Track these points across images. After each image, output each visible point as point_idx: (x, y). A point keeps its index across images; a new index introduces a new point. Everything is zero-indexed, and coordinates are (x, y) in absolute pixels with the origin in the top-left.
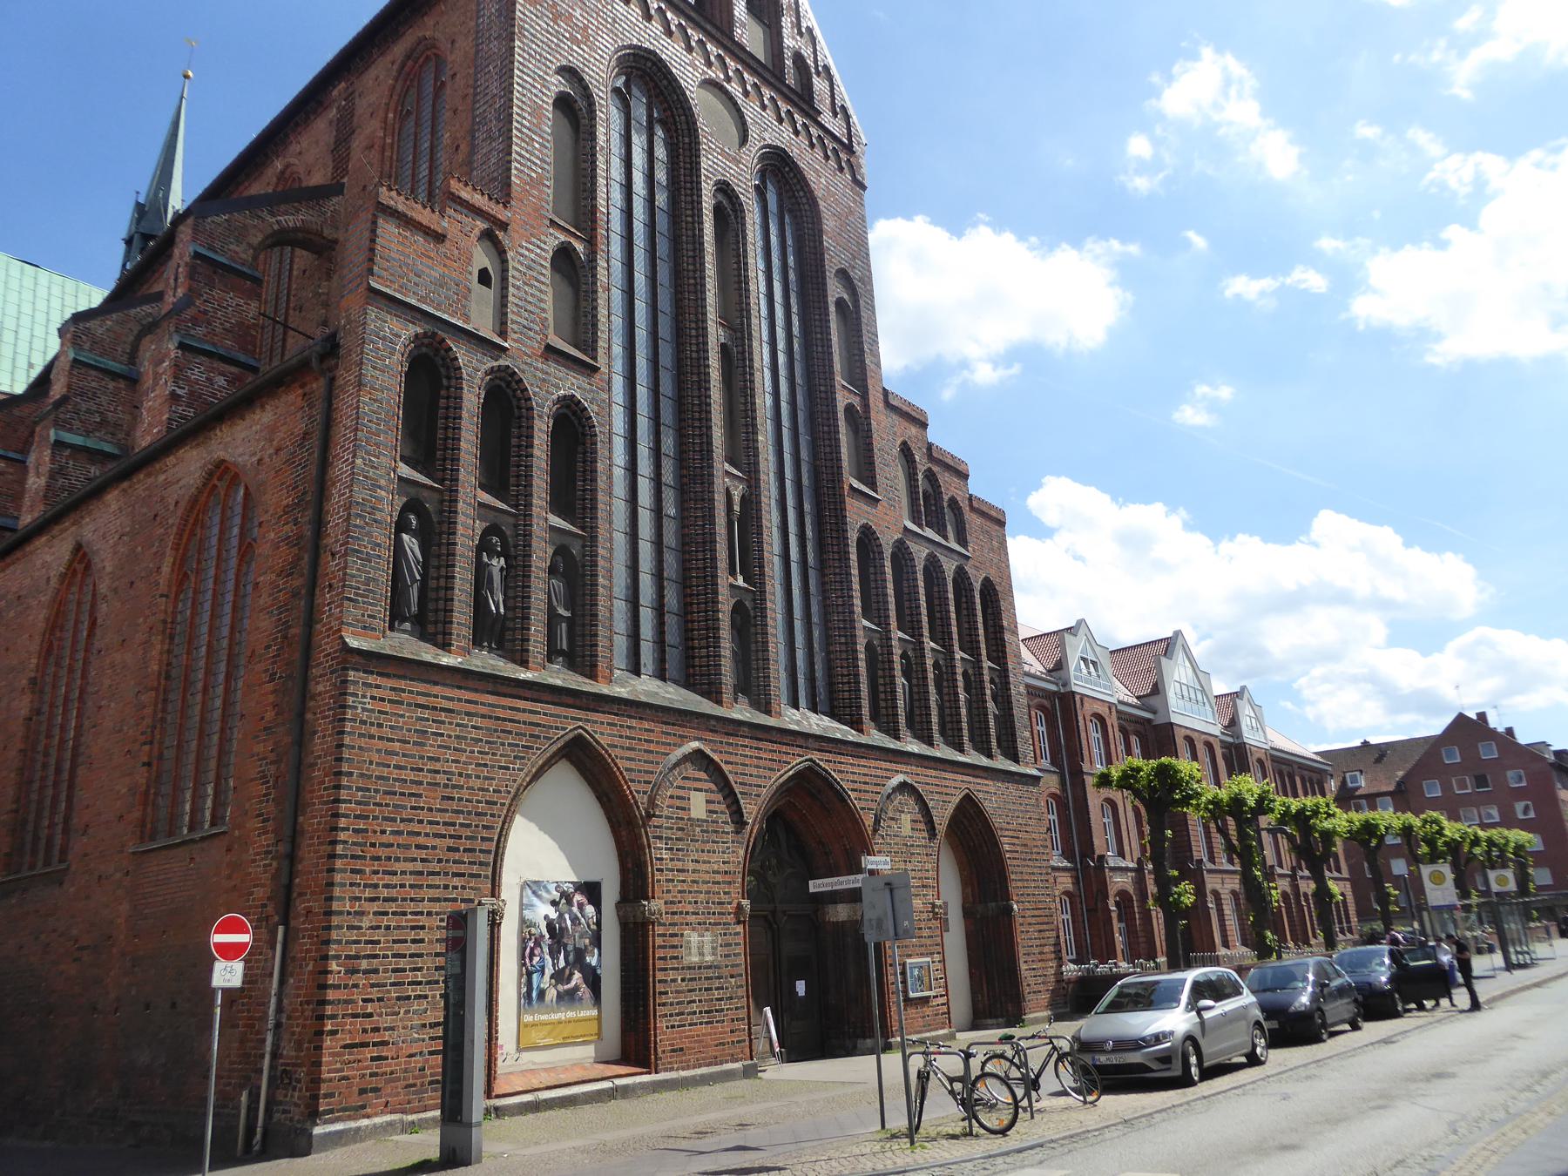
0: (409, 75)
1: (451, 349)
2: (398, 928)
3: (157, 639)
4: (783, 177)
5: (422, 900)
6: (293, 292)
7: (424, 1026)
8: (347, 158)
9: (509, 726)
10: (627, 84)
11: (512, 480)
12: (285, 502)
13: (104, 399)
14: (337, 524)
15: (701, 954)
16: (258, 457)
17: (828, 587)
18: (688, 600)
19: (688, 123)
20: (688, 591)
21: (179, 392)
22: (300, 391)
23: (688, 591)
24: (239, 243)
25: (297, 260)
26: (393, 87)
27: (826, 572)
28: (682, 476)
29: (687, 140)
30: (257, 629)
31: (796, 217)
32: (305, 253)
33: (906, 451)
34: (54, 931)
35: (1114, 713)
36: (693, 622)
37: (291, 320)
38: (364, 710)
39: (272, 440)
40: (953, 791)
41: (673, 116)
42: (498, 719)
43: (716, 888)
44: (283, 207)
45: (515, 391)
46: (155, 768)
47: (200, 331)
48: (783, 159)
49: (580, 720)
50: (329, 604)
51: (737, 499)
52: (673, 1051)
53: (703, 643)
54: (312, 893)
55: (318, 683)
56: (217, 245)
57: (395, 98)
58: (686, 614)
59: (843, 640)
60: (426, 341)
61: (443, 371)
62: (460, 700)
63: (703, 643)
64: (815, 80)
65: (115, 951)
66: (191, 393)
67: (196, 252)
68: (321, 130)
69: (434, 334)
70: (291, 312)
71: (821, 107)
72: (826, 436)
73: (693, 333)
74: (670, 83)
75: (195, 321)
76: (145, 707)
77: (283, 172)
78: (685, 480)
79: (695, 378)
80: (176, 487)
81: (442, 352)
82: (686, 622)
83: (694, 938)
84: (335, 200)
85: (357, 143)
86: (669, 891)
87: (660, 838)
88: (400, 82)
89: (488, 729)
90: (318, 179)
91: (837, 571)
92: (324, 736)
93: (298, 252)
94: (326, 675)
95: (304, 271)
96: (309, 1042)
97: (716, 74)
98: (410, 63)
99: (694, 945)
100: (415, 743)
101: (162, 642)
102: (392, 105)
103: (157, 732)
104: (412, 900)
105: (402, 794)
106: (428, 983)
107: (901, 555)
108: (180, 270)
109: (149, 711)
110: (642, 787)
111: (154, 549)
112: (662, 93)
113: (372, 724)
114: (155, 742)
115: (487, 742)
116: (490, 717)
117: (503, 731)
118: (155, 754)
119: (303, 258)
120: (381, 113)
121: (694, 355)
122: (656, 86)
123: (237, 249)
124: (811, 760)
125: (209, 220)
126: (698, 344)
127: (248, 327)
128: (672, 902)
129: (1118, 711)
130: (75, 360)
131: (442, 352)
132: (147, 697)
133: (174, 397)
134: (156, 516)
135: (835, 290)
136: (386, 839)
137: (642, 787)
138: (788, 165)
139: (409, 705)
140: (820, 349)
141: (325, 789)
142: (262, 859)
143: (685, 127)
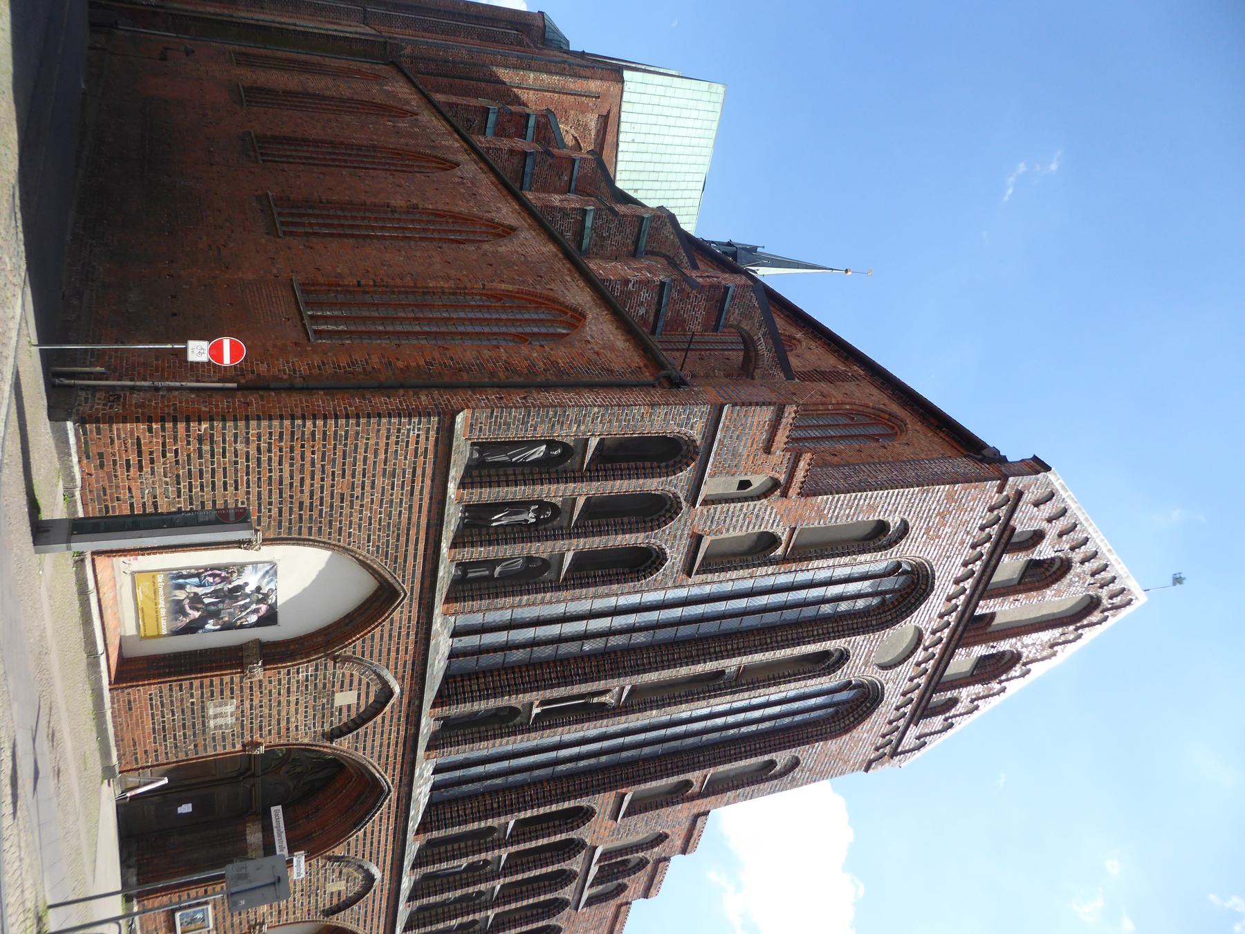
0: (878, 417)
3: (452, 284)
4: (862, 702)
5: (259, 487)
6: (712, 353)
7: (155, 497)
8: (812, 380)
9: (403, 539)
11: (596, 522)
15: (215, 717)
18: (517, 670)
21: (630, 285)
22: (642, 365)
24: (741, 314)
25: (735, 353)
29: (874, 623)
30: (465, 351)
31: (833, 717)
32: (741, 358)
36: (499, 675)
37: (693, 353)
38: (409, 430)
41: (889, 610)
42: (408, 530)
43: (274, 722)
45: (573, 849)
46: (356, 289)
47: (675, 295)
48: (876, 700)
50: (487, 398)
52: (129, 702)
53: (483, 686)
55: (427, 396)
56: (737, 301)
57: (861, 409)
58: (505, 669)
61: (671, 462)
62: (421, 500)
64: (941, 718)
66: (630, 292)
67: (729, 288)
68: (829, 362)
70: (698, 353)
75: (681, 291)
77: (795, 338)
80: (563, 289)
81: (685, 461)
83: (230, 709)
86: (270, 682)
87: (316, 670)
88: (872, 411)
89: (400, 523)
90: (794, 362)
93: (741, 354)
94: (434, 400)
98: (887, 416)
100: (385, 470)
101: (449, 288)
102: (855, 407)
103: (384, 289)
104: (259, 479)
105: (344, 464)
107: (572, 848)
108: (715, 279)
109: (398, 281)
110: (358, 649)
112: (905, 599)
113: (398, 437)
114: (376, 288)
115: (389, 523)
116: (409, 524)
117: (398, 535)
119: (737, 357)
120: (848, 400)
121: (712, 650)
123: (736, 314)
124: (390, 791)
125: (752, 294)
126: (721, 652)
127: (683, 326)
131: (685, 461)
133: (627, 282)
134: (541, 277)
135: (782, 758)
136: (308, 455)
137: (358, 649)
138: (872, 705)
139: (415, 463)
140: (733, 752)
142: (289, 368)
143: (884, 620)
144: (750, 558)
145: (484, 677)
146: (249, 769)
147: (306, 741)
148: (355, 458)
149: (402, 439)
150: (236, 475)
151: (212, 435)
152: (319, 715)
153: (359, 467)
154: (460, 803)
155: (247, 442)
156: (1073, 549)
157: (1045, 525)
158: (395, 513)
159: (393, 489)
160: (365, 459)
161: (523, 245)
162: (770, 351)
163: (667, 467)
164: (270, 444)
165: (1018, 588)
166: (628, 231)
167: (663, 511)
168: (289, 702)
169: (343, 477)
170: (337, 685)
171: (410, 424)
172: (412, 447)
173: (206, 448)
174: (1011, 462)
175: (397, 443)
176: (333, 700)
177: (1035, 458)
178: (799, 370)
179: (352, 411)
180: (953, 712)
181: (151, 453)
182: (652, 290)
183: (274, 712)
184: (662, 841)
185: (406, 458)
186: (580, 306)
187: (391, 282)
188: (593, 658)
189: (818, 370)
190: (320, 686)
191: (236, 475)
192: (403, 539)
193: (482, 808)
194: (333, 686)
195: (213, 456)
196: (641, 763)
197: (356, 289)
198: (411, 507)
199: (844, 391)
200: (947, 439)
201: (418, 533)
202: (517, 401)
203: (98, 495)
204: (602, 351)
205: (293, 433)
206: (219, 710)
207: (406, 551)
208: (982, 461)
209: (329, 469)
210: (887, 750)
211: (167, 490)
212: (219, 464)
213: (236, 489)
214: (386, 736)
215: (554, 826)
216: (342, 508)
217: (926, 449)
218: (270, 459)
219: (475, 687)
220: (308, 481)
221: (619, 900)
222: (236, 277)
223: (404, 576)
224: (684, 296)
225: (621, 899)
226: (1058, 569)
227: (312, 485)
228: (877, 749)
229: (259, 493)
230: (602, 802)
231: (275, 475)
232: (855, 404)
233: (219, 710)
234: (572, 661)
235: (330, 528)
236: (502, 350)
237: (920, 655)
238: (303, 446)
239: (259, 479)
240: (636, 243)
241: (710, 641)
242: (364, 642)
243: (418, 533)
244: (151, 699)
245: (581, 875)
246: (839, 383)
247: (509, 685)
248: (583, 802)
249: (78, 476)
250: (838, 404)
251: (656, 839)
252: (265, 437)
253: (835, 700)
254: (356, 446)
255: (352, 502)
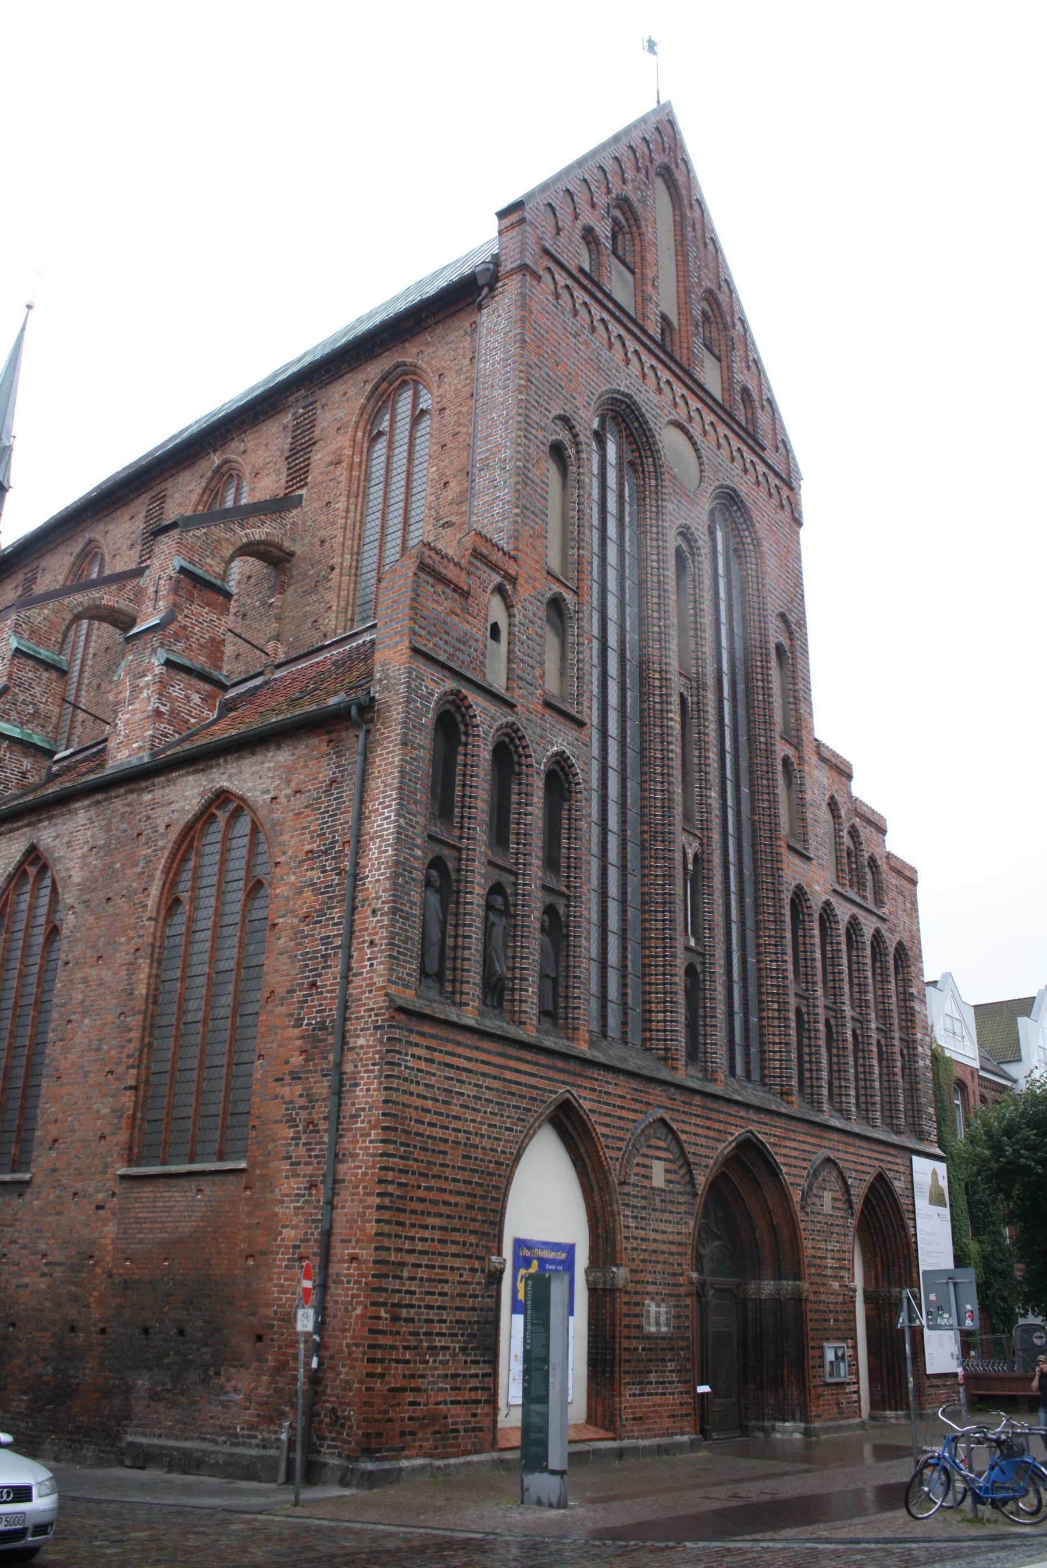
1: (465, 698)
2: (429, 1280)
3: (144, 963)
5: (447, 1255)
7: (446, 1376)
8: (305, 470)
9: (514, 1088)
10: (602, 423)
11: (512, 838)
12: (307, 848)
13: (38, 690)
14: (378, 881)
15: (658, 1324)
16: (272, 794)
17: (762, 949)
18: (647, 961)
19: (655, 465)
20: (647, 952)
21: (163, 709)
23: (647, 952)
24: (213, 556)
26: (364, 407)
27: (761, 933)
28: (643, 832)
29: (653, 482)
30: (277, 971)
33: (833, 805)
34: (14, 1242)
35: (976, 1080)
36: (650, 984)
38: (407, 1067)
39: (288, 782)
40: (867, 1169)
41: (641, 457)
42: (505, 1080)
43: (671, 1259)
44: (251, 520)
45: (517, 747)
46: (141, 1093)
47: (180, 646)
48: (732, 497)
49: (567, 1083)
50: (369, 959)
51: (690, 857)
52: (634, 1419)
53: (661, 1007)
54: (358, 1241)
55: (358, 1036)
57: (366, 417)
58: (644, 975)
59: (775, 1006)
60: (451, 698)
61: (462, 727)
62: (477, 1061)
63: (661, 1007)
64: (759, 413)
65: (98, 1270)
66: (172, 711)
69: (459, 691)
71: (765, 443)
72: (765, 790)
73: (657, 683)
74: (641, 425)
75: (177, 637)
76: (131, 1030)
77: (220, 467)
78: (646, 836)
79: (658, 731)
80: (168, 809)
82: (643, 790)
83: (653, 1308)
84: (294, 512)
85: (319, 457)
86: (633, 1260)
87: (627, 1205)
88: (372, 402)
89: (498, 1090)
91: (772, 933)
92: (368, 1090)
94: (368, 1029)
95: (249, 577)
96: (360, 1382)
97: (681, 415)
98: (384, 385)
99: (652, 1315)
100: (444, 1102)
101: (151, 966)
102: (362, 424)
103: (145, 1056)
104: (440, 1254)
105: (433, 1151)
106: (450, 1335)
107: (827, 913)
109: (135, 1035)
110: (614, 1154)
111: (139, 869)
112: (632, 434)
113: (412, 1082)
114: (143, 1066)
115: (497, 1103)
116: (499, 1079)
117: (510, 1093)
118: (143, 1077)
121: (658, 706)
122: (628, 428)
123: (212, 563)
124: (750, 1132)
126: (661, 695)
128: (636, 1271)
129: (980, 1077)
130: (17, 650)
132: (135, 1021)
133: (158, 713)
134: (139, 834)
136: (421, 1193)
137: (614, 1154)
139: (439, 1063)
141: (371, 1142)
142: (292, 1201)
143: (652, 469)
144: (570, 639)
145: (650, 1003)
146: (731, 1290)
147: (692, 1224)
148: (429, 1137)
149: (416, 1076)
150: (434, 1280)
151: (393, 1305)
152: (670, 1207)
153: (437, 1132)
154: (766, 1048)
155: (402, 1264)
156: (609, 191)
157: (579, 225)
158: (488, 1095)
159: (462, 1094)
160: (432, 1125)
161: (69, 844)
162: (263, 523)
163: (467, 734)
164: (407, 1238)
165: (638, 276)
166: (30, 675)
167: (512, 747)
168: (655, 1241)
169: (445, 1153)
170: (645, 1182)
171: (399, 1065)
172: (423, 1066)
173: (404, 1313)
174: (500, 248)
175: (418, 1083)
176: (659, 1189)
177: (502, 215)
178: (283, 481)
179: (378, 1134)
180: (755, 396)
181: (404, 1376)
182: (172, 679)
183: (662, 1258)
184: (836, 804)
185: (434, 1075)
186: (204, 793)
187: (135, 1045)
188: (646, 862)
189: (287, 454)
190: (643, 1202)
191: (434, 1280)
192: (514, 1088)
193: (776, 1023)
194: (645, 1187)
195: (412, 1306)
196: (756, 818)
197: (141, 1093)
198: (483, 1075)
199: (333, 431)
200: (441, 317)
201: (510, 1069)
202: (378, 921)
203: (441, 1439)
204: (293, 784)
205: (398, 1210)
206: (652, 1321)
207: (526, 1085)
208: (492, 289)
209: (436, 1169)
210: (785, 493)
211: (441, 1362)
212: (421, 1299)
213: (446, 1281)
214: (699, 1131)
215: (804, 936)
216: (476, 1159)
217: (452, 353)
218: (422, 1239)
219: (661, 1016)
220: (446, 1197)
221: (884, 867)
222: (110, 1247)
223: (550, 1091)
224: (180, 635)
225: (881, 862)
226: (624, 213)
227: (451, 1192)
228: (782, 506)
229: (454, 1255)
230: (793, 871)
231: (438, 1235)
232: (357, 423)
233: (652, 1321)
234: (646, 889)
235: (494, 1174)
236: (281, 920)
237: (695, 429)
238: (412, 1199)
239: (440, 1254)
240: (48, 666)
241: (645, 706)
242: (607, 1147)
243: (510, 1069)
244: (634, 1395)
245: (856, 910)
246: (317, 434)
247: (664, 974)
248: (787, 897)
249: (420, 1461)
250: (354, 446)
251: (832, 811)
252: (399, 1243)
253: (614, 462)
254: (417, 1134)
255: (472, 1146)
